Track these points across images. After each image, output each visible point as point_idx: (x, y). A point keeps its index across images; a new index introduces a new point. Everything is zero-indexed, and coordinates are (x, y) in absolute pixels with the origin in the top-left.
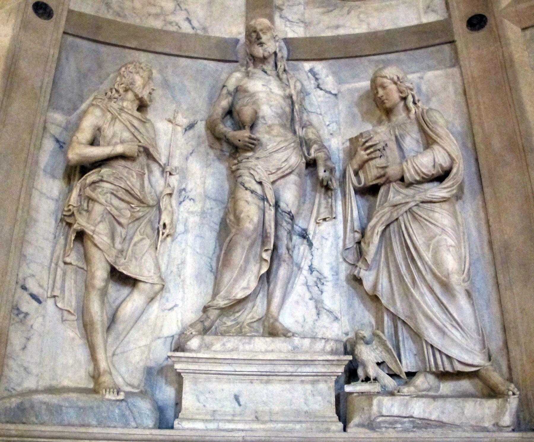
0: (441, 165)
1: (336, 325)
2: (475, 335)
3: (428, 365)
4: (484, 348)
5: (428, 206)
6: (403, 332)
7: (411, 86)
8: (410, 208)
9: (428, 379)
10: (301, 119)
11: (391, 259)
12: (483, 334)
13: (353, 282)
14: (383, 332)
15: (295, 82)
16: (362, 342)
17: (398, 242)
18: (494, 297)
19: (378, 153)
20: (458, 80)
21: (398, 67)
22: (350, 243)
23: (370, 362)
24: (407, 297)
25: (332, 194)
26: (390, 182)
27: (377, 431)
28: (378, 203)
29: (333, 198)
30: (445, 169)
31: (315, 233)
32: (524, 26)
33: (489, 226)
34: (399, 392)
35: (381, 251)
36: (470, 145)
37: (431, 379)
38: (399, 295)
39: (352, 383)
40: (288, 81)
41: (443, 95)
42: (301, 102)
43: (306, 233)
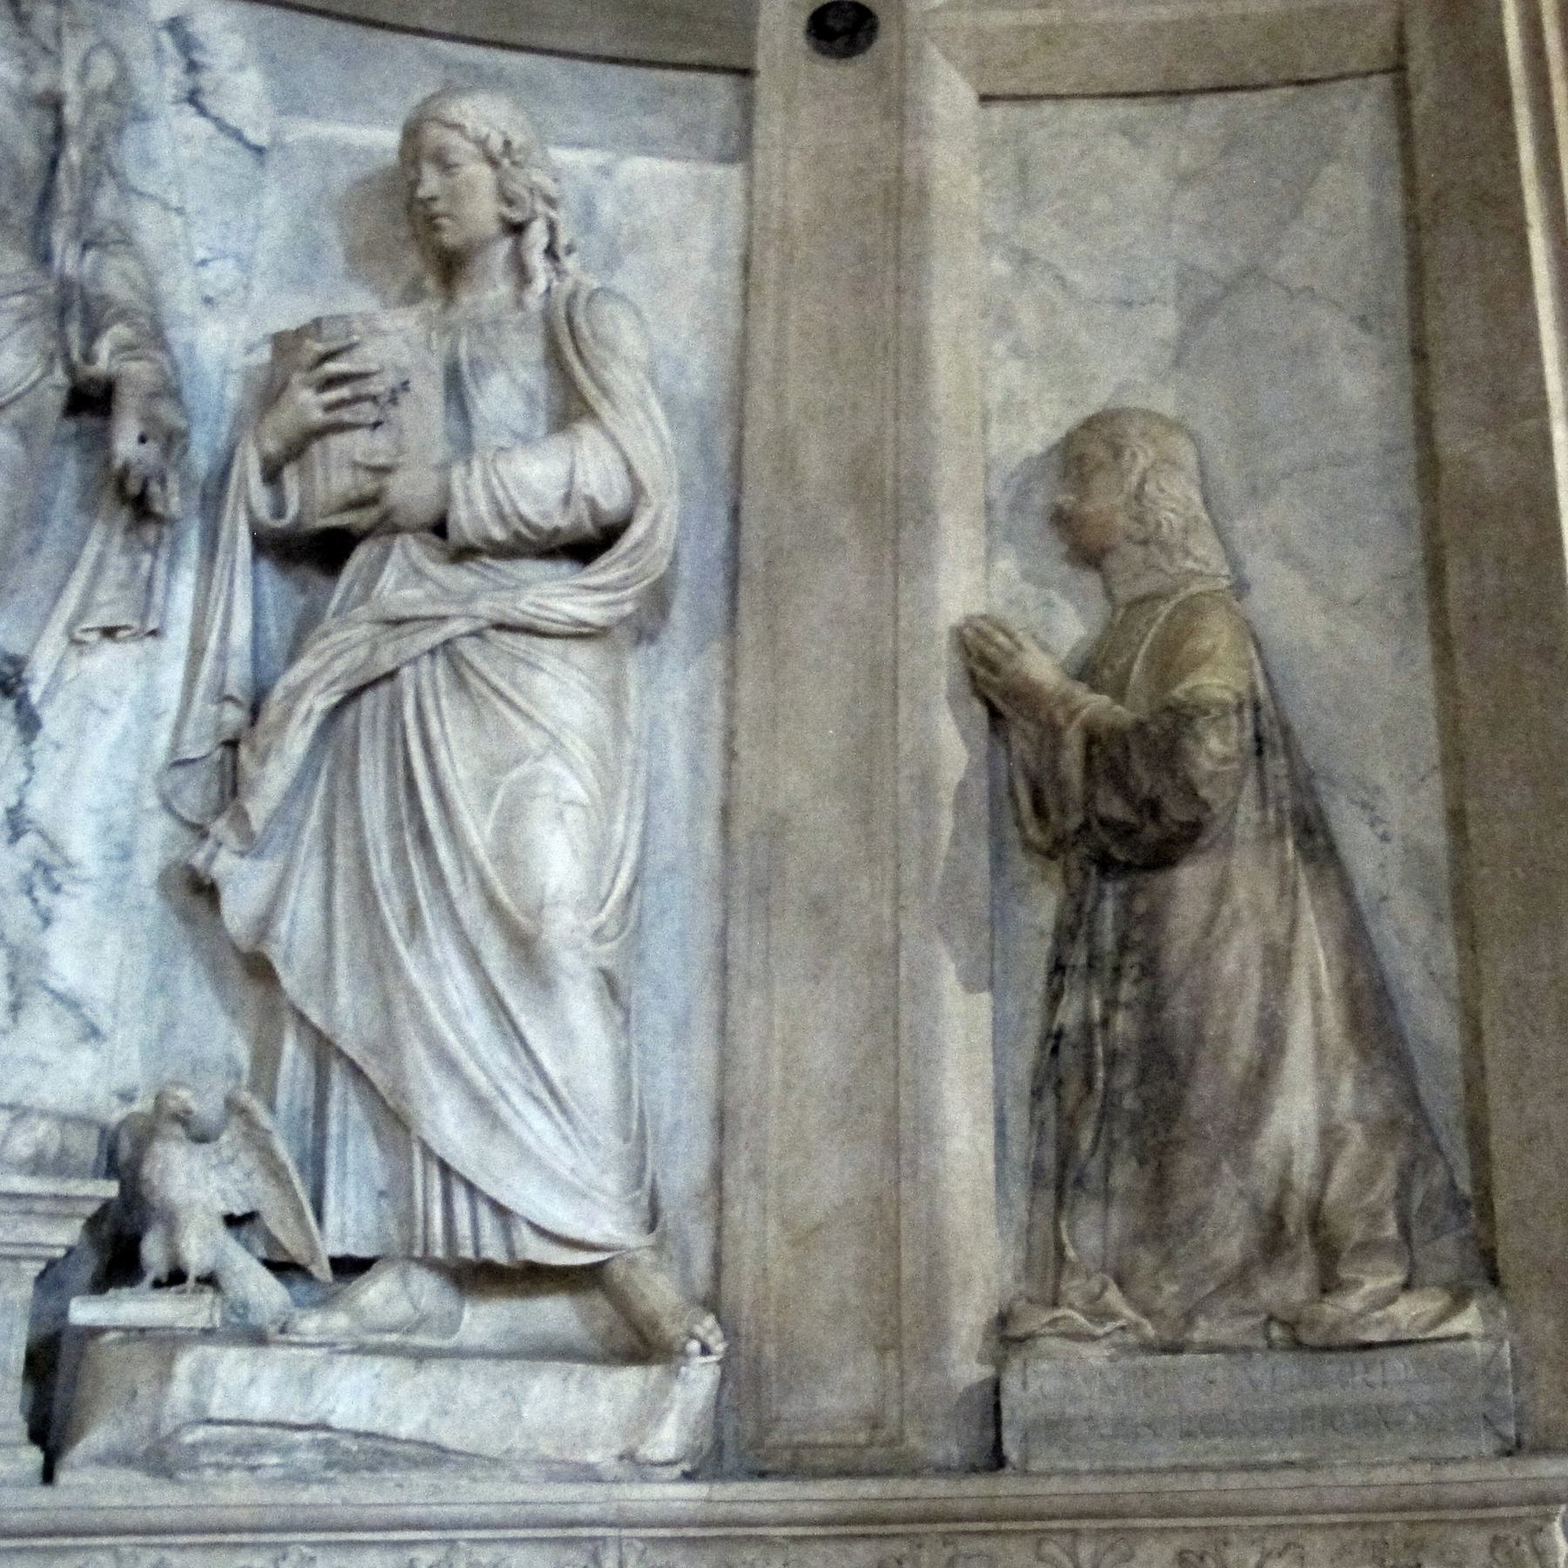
0: (592, 502)
1: (86, 1056)
2: (611, 1141)
3: (419, 1231)
4: (639, 1183)
5: (521, 642)
6: (345, 1105)
7: (552, 189)
8: (447, 643)
9: (414, 1287)
10: (84, 208)
11: (343, 822)
12: (642, 1137)
13: (182, 895)
14: (271, 1107)
15: (93, 49)
16: (178, 1130)
17: (381, 765)
18: (706, 1005)
19: (367, 412)
20: (734, 218)
21: (517, 104)
22: (199, 741)
23: (198, 1209)
24: (379, 969)
25: (160, 537)
26: (396, 530)
27: (180, 1483)
28: (334, 604)
29: (164, 553)
30: (606, 521)
31: (57, 675)
32: (985, 89)
33: (731, 754)
34: (283, 1330)
35: (312, 789)
36: (723, 460)
37: (428, 1289)
38: (351, 964)
39: (112, 1292)
40: (58, 33)
41: (668, 256)
42: (99, 136)
43: (18, 674)
